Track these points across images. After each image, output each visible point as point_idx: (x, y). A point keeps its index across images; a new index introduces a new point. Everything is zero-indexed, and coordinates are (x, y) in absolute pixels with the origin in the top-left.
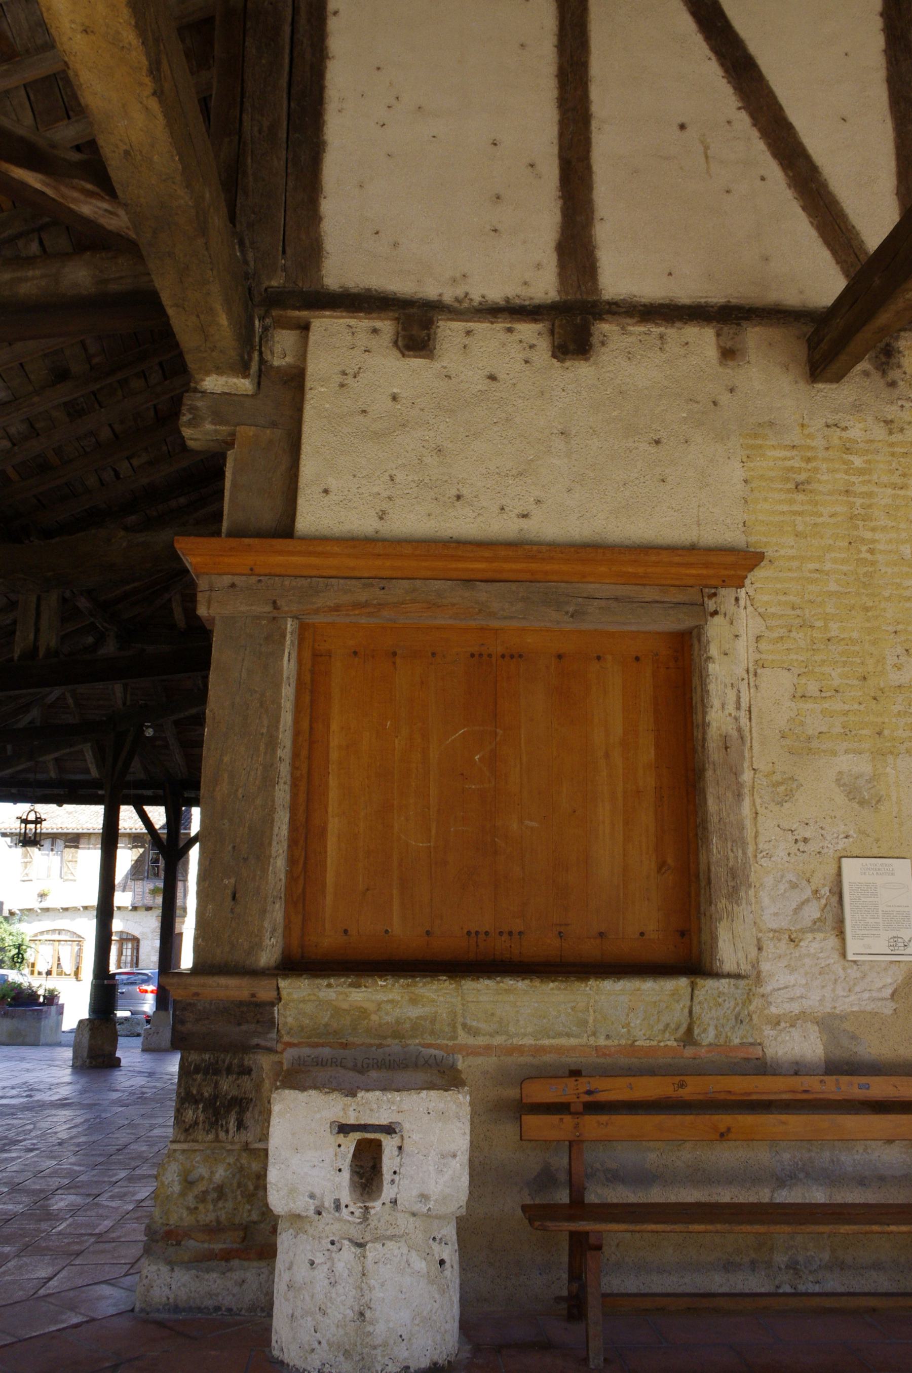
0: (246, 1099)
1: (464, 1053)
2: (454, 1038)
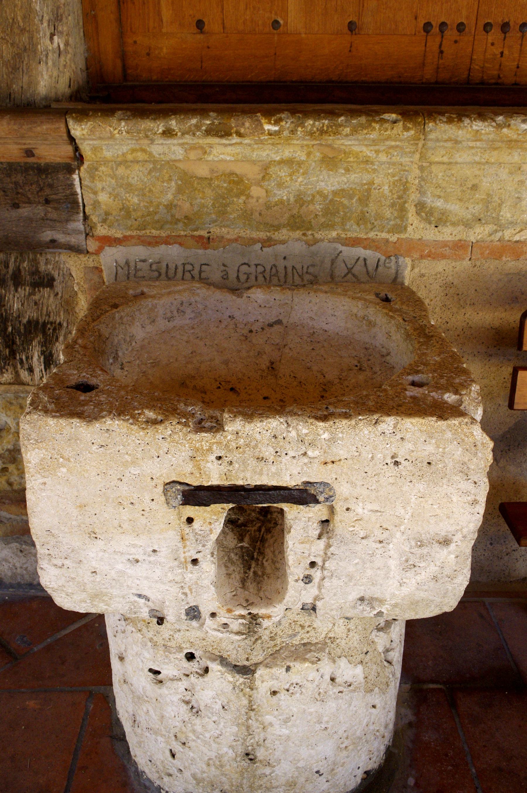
0: (51, 323)
1: (416, 255)
2: (401, 228)
